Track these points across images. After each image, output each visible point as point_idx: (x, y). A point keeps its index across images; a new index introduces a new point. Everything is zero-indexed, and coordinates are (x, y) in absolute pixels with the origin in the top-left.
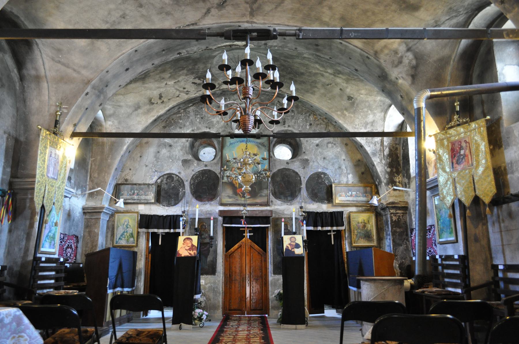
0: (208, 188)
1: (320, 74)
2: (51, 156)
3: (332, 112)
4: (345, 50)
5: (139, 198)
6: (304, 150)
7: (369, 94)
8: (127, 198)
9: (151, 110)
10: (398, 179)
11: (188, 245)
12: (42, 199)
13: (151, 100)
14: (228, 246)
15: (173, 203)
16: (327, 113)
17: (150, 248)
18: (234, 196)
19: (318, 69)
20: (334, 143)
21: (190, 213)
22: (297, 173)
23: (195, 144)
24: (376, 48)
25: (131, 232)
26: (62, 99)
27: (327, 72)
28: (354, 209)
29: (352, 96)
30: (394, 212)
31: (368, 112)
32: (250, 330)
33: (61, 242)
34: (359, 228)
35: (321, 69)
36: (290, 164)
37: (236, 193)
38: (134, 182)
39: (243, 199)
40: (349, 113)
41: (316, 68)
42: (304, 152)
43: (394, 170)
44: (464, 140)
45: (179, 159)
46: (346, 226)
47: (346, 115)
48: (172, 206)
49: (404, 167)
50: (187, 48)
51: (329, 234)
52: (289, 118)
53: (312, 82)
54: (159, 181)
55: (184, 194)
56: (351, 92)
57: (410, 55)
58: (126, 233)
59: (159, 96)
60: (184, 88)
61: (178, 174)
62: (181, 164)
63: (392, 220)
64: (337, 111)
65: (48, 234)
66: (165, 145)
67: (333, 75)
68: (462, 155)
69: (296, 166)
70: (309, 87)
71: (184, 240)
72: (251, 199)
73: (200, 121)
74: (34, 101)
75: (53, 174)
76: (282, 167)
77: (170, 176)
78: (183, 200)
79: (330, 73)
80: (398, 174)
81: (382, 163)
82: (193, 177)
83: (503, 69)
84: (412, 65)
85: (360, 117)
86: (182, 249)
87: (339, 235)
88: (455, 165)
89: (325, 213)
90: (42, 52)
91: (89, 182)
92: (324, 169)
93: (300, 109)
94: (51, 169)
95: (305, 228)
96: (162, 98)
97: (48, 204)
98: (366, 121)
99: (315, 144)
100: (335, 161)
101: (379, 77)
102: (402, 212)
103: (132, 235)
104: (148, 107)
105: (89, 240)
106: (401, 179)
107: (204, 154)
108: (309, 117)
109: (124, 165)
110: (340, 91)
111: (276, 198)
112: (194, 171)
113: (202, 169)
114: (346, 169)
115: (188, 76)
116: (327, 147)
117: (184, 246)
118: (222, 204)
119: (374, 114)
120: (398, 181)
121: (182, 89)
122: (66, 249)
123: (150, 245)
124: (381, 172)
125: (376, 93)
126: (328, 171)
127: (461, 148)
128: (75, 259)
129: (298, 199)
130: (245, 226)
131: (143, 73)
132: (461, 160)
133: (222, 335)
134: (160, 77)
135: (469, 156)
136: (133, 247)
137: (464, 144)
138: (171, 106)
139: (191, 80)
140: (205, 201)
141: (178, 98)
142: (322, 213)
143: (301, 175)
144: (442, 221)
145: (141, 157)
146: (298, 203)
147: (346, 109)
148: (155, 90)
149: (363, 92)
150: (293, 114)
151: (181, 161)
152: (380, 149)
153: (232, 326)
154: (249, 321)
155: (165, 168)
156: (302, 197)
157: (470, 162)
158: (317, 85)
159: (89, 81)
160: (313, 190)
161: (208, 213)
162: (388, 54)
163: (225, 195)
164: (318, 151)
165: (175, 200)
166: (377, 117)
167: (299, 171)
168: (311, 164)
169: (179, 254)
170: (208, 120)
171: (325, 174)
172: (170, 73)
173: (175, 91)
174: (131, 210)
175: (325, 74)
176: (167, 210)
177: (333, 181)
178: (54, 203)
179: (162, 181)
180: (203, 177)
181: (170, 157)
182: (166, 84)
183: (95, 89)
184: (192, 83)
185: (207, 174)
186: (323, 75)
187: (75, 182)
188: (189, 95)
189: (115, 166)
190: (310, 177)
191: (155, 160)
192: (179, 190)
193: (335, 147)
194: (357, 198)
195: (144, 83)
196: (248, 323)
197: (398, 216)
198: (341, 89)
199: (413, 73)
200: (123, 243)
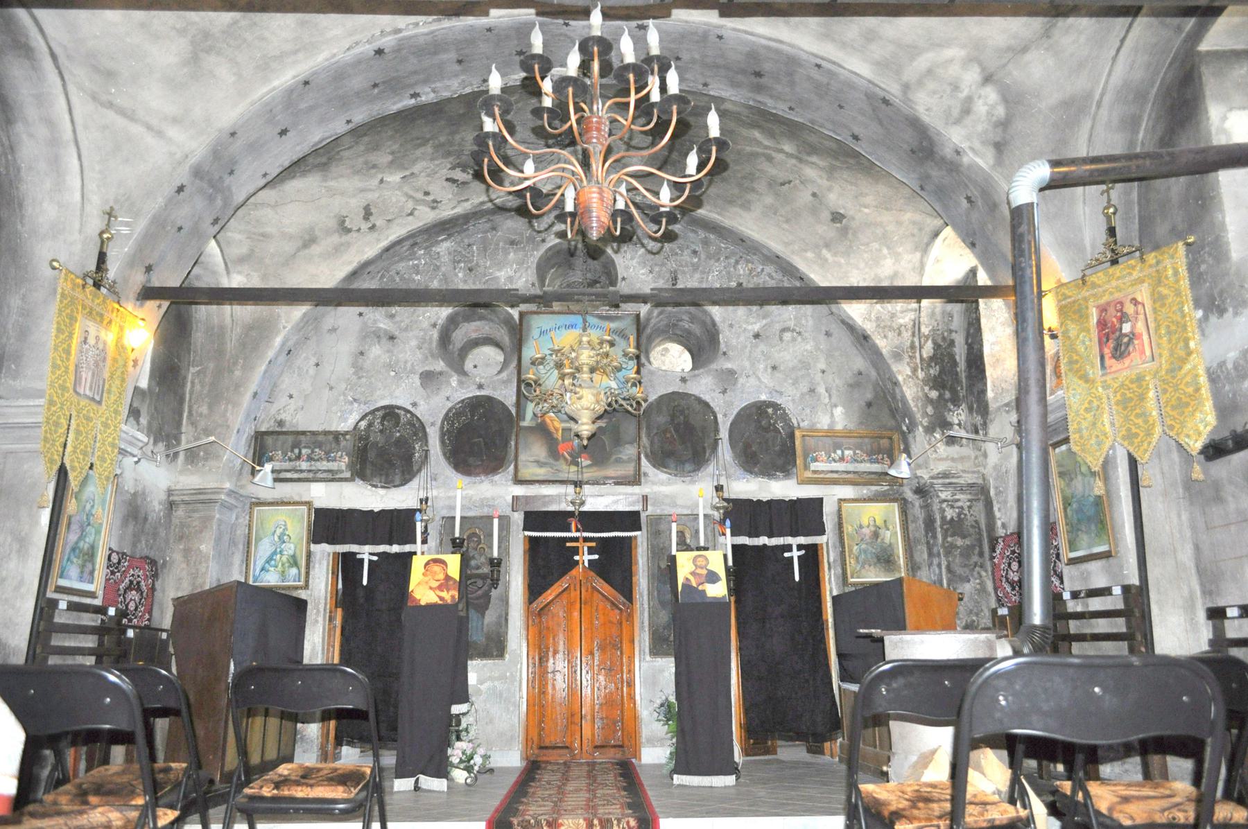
0: (486, 444)
1: (764, 155)
2: (85, 341)
3: (793, 252)
4: (828, 84)
5: (313, 468)
6: (723, 347)
7: (885, 205)
8: (283, 468)
9: (342, 248)
10: (959, 416)
11: (437, 578)
12: (61, 450)
13: (344, 222)
14: (535, 588)
15: (397, 481)
16: (780, 254)
17: (340, 593)
18: (551, 461)
19: (759, 143)
20: (798, 330)
21: (440, 504)
22: (707, 405)
23: (454, 335)
24: (905, 78)
25: (291, 552)
26: (116, 201)
27: (781, 151)
28: (847, 492)
29: (842, 211)
30: (949, 497)
31: (880, 250)
32: (593, 791)
33: (113, 573)
34: (862, 540)
35: (766, 143)
36: (688, 383)
37: (554, 453)
38: (300, 429)
39: (573, 468)
40: (835, 254)
41: (755, 139)
42: (725, 353)
43: (948, 395)
44: (1130, 297)
45: (412, 371)
46: (831, 535)
47: (826, 260)
48: (395, 486)
49: (970, 387)
50: (434, 82)
51: (786, 555)
52: (686, 269)
53: (744, 178)
54: (363, 424)
55: (426, 457)
56: (840, 202)
57: (991, 94)
58: (278, 556)
59: (362, 213)
60: (427, 194)
61: (410, 408)
62: (418, 382)
63: (943, 518)
64: (806, 251)
65: (77, 543)
66: (379, 337)
67: (797, 158)
68: (1126, 335)
69: (704, 387)
70: (736, 191)
71: (427, 564)
72: (595, 469)
73: (465, 276)
74: (45, 205)
75: (91, 388)
76: (670, 390)
77: (390, 413)
78: (422, 473)
79: (787, 153)
80: (957, 405)
81: (917, 377)
82: (447, 414)
83: (1224, 118)
84: (994, 119)
85: (862, 265)
86: (421, 587)
87: (812, 556)
88: (1108, 362)
89: (780, 502)
90: (66, 77)
91: (187, 425)
92: (774, 393)
93: (713, 249)
94: (86, 375)
95: (729, 540)
96: (371, 218)
97: (76, 464)
98: (876, 275)
99: (751, 334)
100: (800, 373)
101: (913, 151)
102: (969, 497)
103: (294, 562)
104: (335, 239)
105: (184, 572)
106: (963, 417)
107: (475, 367)
108: (735, 267)
109: (275, 385)
110: (811, 198)
111: (654, 466)
112: (451, 399)
113: (471, 395)
114: (827, 395)
115: (436, 162)
116: (781, 339)
117: (427, 579)
118: (518, 481)
119: (897, 257)
120: (957, 422)
121: (420, 196)
122: (125, 592)
123: (340, 586)
124: (916, 399)
125: (902, 201)
126: (784, 399)
127: (1123, 318)
128: (149, 620)
129: (711, 468)
130: (578, 534)
131: (324, 143)
132: (1123, 348)
133: (524, 800)
134: (366, 163)
135: (1145, 337)
136: (296, 588)
137: (1130, 309)
138: (393, 237)
139: (445, 172)
140: (477, 475)
141: (411, 218)
142: (770, 502)
143: (717, 409)
144: (1074, 506)
145: (317, 365)
146: (709, 479)
147: (827, 246)
148: (354, 196)
149: (869, 200)
150: (696, 260)
151: (418, 376)
152: (913, 342)
153: (549, 783)
154: (589, 772)
155: (378, 393)
156: (721, 462)
157: (1148, 353)
158: (755, 185)
159: (187, 156)
160: (747, 446)
161: (483, 502)
162: (934, 92)
163: (531, 456)
164: (759, 350)
165: (403, 472)
166: (903, 263)
167: (713, 399)
168: (741, 381)
169: (415, 599)
170: (485, 275)
171: (776, 406)
172: (392, 153)
173: (404, 199)
174: (292, 497)
175: (774, 154)
176: (382, 497)
177: (796, 425)
178: (92, 465)
179: (370, 425)
180: (473, 416)
181: (390, 367)
182: (382, 181)
183: (202, 179)
184: (447, 180)
185: (483, 406)
186: (770, 159)
187: (150, 423)
188: (437, 211)
189: (253, 387)
190: (739, 414)
191: (354, 373)
192: (414, 448)
193: (799, 339)
194: (857, 465)
195: (325, 179)
196: (589, 777)
197: (958, 508)
198: (814, 195)
199: (998, 139)
200: (271, 579)
